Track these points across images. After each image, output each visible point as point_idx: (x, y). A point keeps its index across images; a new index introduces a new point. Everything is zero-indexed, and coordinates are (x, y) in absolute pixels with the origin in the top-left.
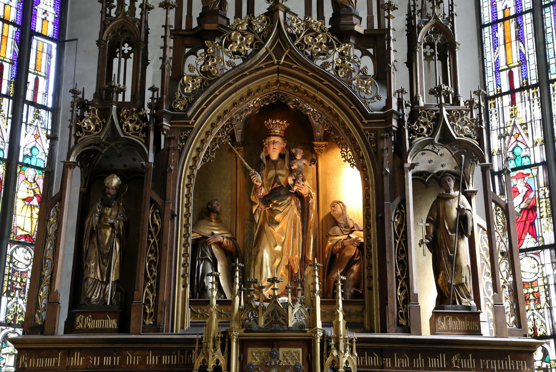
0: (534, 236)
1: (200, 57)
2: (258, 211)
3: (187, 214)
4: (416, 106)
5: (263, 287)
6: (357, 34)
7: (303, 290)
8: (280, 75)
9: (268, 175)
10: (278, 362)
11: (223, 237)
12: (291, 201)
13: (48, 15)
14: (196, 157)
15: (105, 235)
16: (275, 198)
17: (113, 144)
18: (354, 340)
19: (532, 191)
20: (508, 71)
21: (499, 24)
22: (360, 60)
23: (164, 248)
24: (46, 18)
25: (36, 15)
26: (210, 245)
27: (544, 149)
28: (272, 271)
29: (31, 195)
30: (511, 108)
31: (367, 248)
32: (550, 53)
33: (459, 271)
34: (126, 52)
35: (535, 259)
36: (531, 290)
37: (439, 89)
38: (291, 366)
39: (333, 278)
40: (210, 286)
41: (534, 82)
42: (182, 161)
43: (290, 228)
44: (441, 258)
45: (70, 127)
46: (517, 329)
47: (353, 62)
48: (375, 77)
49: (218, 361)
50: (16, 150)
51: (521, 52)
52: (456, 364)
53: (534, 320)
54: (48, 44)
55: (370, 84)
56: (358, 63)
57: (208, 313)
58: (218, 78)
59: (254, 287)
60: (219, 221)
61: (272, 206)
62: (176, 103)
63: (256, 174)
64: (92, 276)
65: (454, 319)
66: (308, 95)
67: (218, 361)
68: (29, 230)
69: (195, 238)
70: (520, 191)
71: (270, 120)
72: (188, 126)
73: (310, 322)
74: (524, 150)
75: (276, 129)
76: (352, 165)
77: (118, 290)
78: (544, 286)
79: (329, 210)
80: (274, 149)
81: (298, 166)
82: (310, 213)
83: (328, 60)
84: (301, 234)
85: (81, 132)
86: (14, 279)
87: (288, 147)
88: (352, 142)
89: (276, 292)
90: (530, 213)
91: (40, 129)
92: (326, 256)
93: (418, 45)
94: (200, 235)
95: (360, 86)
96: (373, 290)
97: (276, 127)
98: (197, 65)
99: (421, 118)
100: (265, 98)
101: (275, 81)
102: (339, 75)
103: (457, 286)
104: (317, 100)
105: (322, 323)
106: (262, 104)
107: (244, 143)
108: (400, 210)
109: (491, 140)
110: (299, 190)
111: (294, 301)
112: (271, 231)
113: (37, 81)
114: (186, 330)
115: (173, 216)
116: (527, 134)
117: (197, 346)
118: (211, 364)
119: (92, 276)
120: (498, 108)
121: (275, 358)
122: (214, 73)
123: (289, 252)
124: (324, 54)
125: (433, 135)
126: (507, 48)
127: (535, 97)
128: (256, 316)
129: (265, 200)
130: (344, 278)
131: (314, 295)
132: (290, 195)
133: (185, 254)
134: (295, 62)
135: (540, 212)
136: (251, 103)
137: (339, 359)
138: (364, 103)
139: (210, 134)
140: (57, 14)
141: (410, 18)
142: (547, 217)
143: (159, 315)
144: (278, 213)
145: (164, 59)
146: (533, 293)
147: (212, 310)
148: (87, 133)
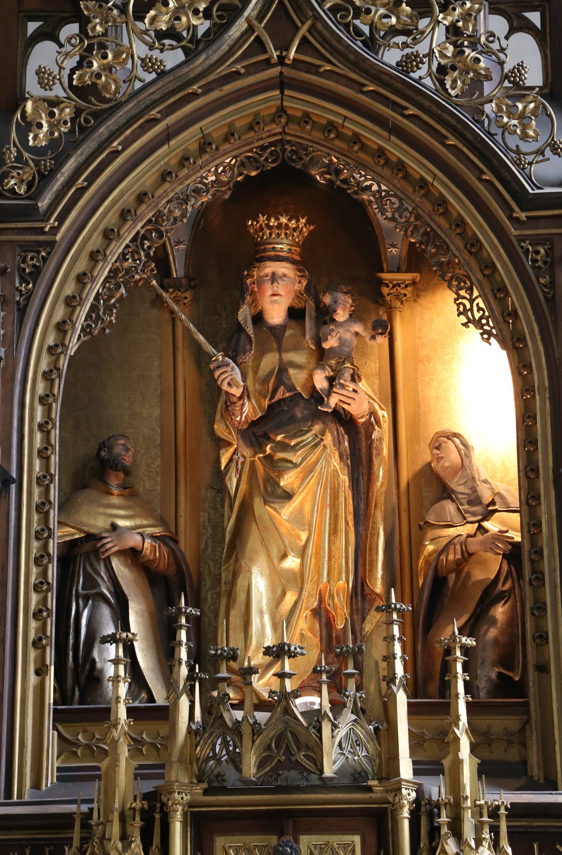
1: (68, 48)
2: (234, 464)
3: (45, 477)
5: (251, 671)
7: (361, 674)
8: (286, 92)
9: (258, 366)
11: (141, 534)
12: (323, 434)
14: (64, 322)
16: (280, 427)
18: (502, 811)
22: (504, 46)
26: (109, 557)
28: (275, 626)
31: (530, 559)
39: (441, 641)
40: (110, 670)
42: (27, 333)
47: (488, 52)
48: (546, 91)
55: (534, 112)
56: (501, 55)
57: (105, 743)
58: (120, 105)
59: (230, 670)
61: (271, 448)
63: (227, 365)
66: (364, 147)
69: (68, 539)
71: (262, 219)
72: (42, 238)
73: (380, 764)
75: (278, 240)
76: (487, 335)
79: (426, 456)
80: (274, 295)
81: (340, 339)
82: (375, 467)
84: (351, 524)
88: (486, 272)
89: (288, 682)
92: (421, 582)
95: (505, 120)
96: (549, 672)
97: (278, 235)
98: (61, 68)
100: (248, 158)
101: (274, 110)
102: (446, 90)
104: (387, 161)
105: (414, 763)
106: (240, 174)
110: (345, 406)
112: (271, 518)
122: (108, 91)
123: (319, 573)
124: (407, 33)
128: (235, 748)
129: (253, 434)
130: (469, 642)
131: (389, 688)
132: (319, 418)
133: (41, 583)
134: (328, 55)
136: (209, 171)
138: (517, 164)
139: (100, 257)
144: (290, 469)
147: (115, 734)
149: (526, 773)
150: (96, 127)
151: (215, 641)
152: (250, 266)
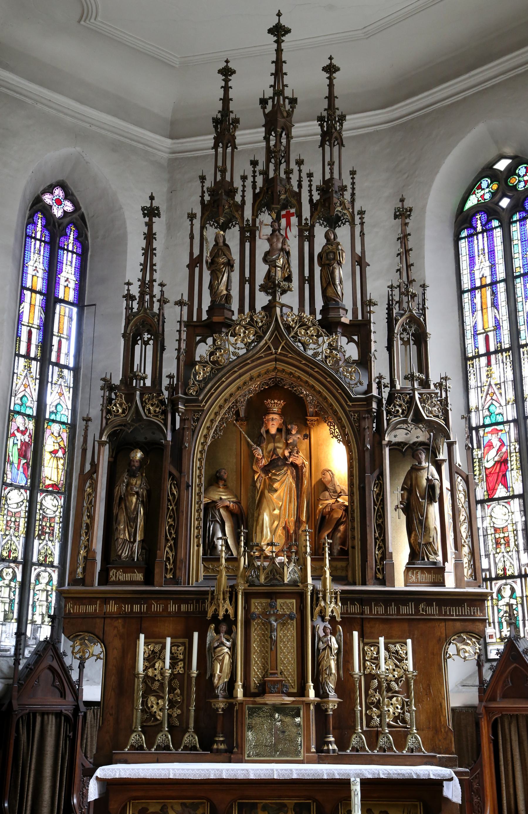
0: (506, 486)
4: (393, 389)
6: (344, 324)
10: (276, 611)
13: (69, 282)
14: (206, 435)
15: (132, 501)
16: (274, 468)
17: (137, 425)
18: (339, 593)
19: (505, 445)
20: (484, 334)
21: (477, 291)
23: (181, 514)
24: (67, 285)
25: (59, 283)
27: (515, 408)
29: (57, 448)
30: (487, 369)
32: (521, 320)
33: (428, 532)
34: (146, 339)
35: (506, 507)
36: (502, 535)
37: (412, 375)
38: (286, 614)
40: (220, 548)
41: (507, 346)
42: (195, 438)
43: (287, 494)
44: (413, 521)
45: (102, 410)
46: (473, 581)
49: (227, 611)
50: (43, 407)
51: (495, 318)
52: (423, 611)
53: (504, 561)
54: (69, 308)
55: (354, 372)
58: (225, 367)
60: (226, 486)
62: (189, 389)
64: (122, 537)
65: (422, 573)
67: (227, 611)
68: (56, 480)
70: (494, 446)
74: (498, 408)
77: (143, 548)
78: (513, 531)
79: (320, 476)
83: (318, 350)
85: (111, 415)
86: (44, 524)
87: (285, 423)
90: (503, 466)
91: (63, 387)
93: (395, 335)
94: (210, 499)
99: (397, 401)
103: (425, 545)
107: (247, 418)
108: (378, 480)
109: (470, 397)
111: (289, 562)
112: (270, 497)
113: (60, 342)
114: (201, 582)
115: (188, 486)
116: (501, 394)
117: (210, 597)
118: (222, 613)
119: (122, 537)
120: (476, 369)
121: (273, 608)
122: (221, 362)
123: (285, 516)
125: (407, 416)
126: (484, 314)
127: (508, 360)
135: (511, 465)
137: (325, 609)
138: (349, 388)
140: (77, 280)
141: (390, 309)
142: (517, 469)
143: (177, 571)
144: (276, 482)
145: (179, 350)
146: (504, 538)
147: (221, 568)
148: (115, 416)
149: (347, 579)
150: (218, 374)
151: (252, 541)
152: (265, 415)
